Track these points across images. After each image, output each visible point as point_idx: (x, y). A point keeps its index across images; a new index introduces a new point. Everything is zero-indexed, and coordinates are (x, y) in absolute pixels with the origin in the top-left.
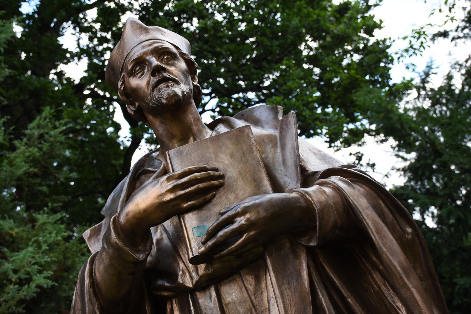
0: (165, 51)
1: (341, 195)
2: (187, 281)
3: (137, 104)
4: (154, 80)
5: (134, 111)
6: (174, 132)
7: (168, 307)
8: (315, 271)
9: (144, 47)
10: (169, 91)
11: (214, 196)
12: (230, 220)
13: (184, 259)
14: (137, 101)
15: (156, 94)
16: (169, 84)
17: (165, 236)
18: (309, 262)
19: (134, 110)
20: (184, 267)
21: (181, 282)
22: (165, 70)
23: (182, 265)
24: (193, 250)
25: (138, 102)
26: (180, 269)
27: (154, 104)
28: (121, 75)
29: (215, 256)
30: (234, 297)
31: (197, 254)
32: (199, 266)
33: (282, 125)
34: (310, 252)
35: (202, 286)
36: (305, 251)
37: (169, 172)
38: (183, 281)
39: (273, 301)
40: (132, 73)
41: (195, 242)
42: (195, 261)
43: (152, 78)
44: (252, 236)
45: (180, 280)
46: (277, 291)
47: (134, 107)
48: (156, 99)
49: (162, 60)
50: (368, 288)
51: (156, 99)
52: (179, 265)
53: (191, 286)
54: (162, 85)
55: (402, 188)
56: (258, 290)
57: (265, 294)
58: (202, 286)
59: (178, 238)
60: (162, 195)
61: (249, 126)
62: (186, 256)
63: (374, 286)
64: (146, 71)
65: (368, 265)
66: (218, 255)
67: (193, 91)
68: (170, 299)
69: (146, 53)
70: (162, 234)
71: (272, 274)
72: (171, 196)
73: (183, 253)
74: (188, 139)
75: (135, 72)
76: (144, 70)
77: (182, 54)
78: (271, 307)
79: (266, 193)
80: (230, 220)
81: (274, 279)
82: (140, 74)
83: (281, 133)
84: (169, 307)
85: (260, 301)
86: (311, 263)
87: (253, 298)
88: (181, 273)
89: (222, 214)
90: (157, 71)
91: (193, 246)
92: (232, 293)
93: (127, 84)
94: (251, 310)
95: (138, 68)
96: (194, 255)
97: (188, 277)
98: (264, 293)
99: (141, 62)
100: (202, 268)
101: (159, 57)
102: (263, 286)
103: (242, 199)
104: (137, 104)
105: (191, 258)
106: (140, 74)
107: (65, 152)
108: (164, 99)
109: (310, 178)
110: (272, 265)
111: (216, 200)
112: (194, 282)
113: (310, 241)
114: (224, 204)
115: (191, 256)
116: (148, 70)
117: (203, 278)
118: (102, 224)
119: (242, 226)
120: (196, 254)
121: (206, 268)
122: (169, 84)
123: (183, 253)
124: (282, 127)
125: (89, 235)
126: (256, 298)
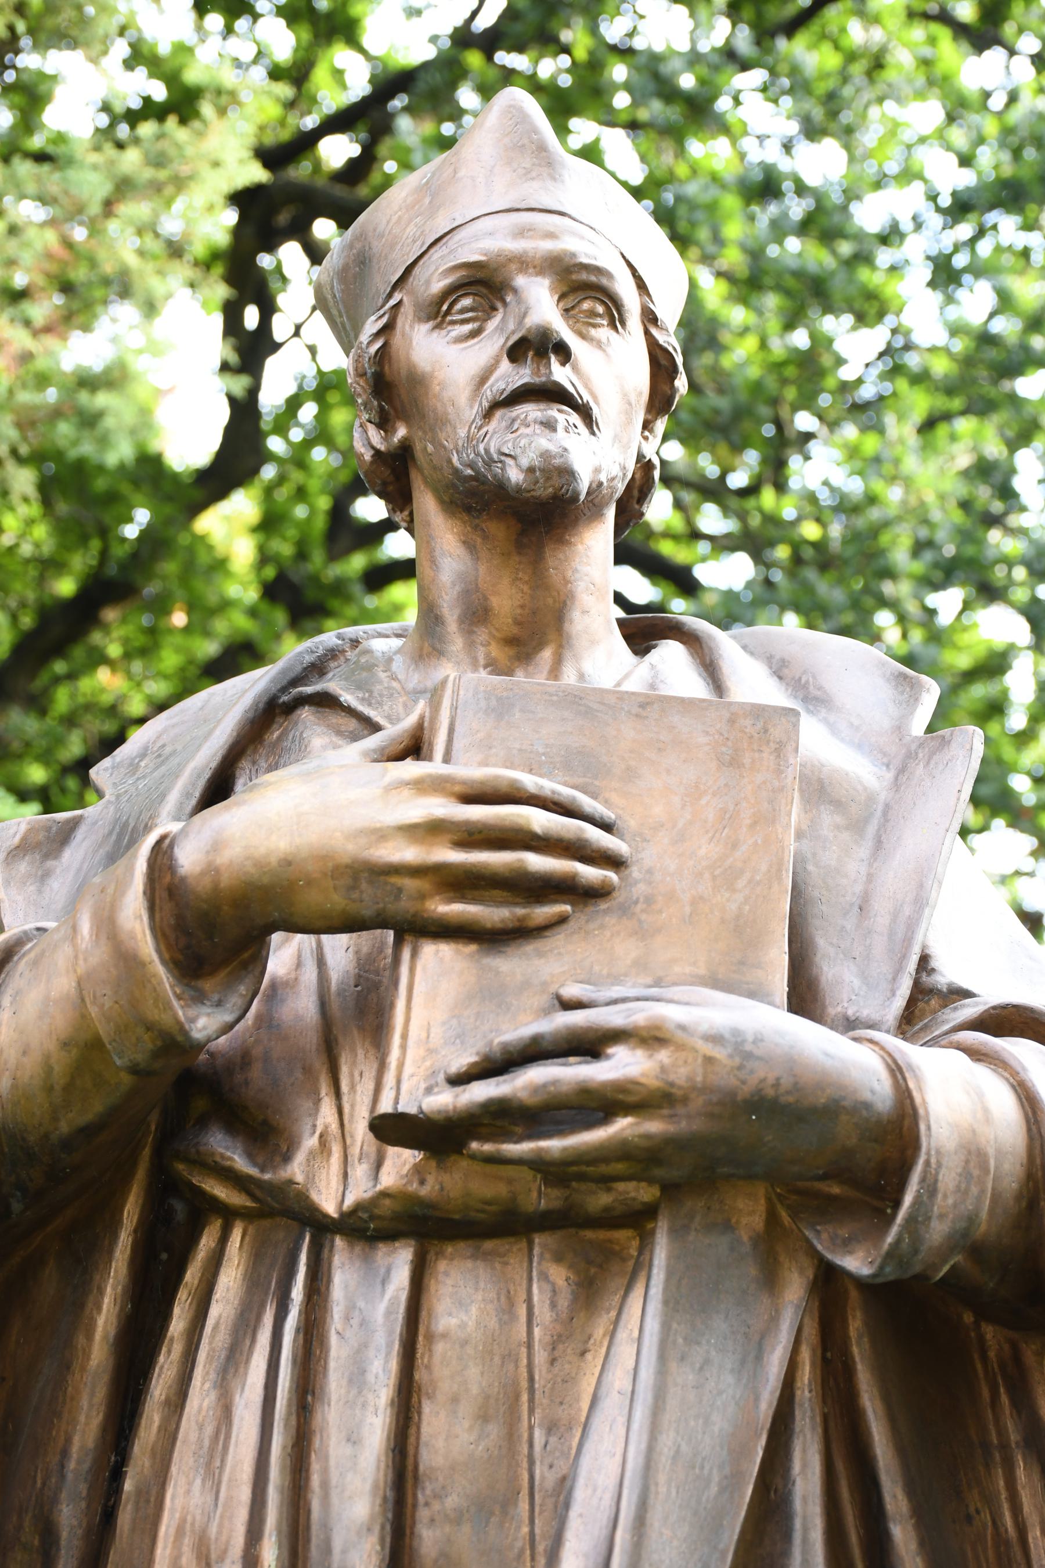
0: (593, 278)
1: (1034, 1128)
2: (322, 1185)
3: (401, 432)
4: (512, 376)
5: (377, 453)
6: (495, 601)
7: (204, 1241)
8: (813, 1364)
9: (521, 232)
10: (544, 442)
11: (562, 920)
12: (589, 1045)
13: (345, 1099)
14: (407, 419)
15: (497, 436)
16: (561, 418)
17: (310, 975)
18: (806, 1320)
19: (382, 447)
20: (334, 1127)
21: (299, 1178)
22: (564, 352)
23: (327, 1114)
24: (405, 1087)
25: (409, 426)
26: (315, 1126)
27: (471, 465)
28: (390, 296)
29: (474, 1145)
30: (471, 1324)
31: (412, 1110)
32: (392, 1151)
33: (910, 756)
34: (828, 1280)
35: (369, 1227)
36: (810, 1274)
37: (430, 758)
38: (310, 1177)
39: (612, 1406)
40: (437, 312)
41: (424, 1059)
42: (392, 1129)
43: (505, 365)
44: (647, 1136)
45: (296, 1170)
46: (647, 1375)
47: (385, 439)
48: (487, 451)
49: (567, 310)
50: (978, 1512)
51: (487, 451)
52: (317, 1110)
53: (330, 1208)
54: (531, 411)
55: (53, 47)
56: (572, 1337)
57: (594, 1362)
58: (369, 1227)
59: (363, 1013)
60: (381, 835)
61: (795, 713)
62: (366, 1087)
63: (1002, 1515)
64: (492, 325)
65: (1010, 1425)
66: (488, 1147)
67: (629, 476)
68: (229, 1215)
69: (524, 263)
70: (299, 965)
71: (655, 1305)
72: (409, 853)
73: (352, 1075)
74: (540, 646)
75: (448, 312)
76: (488, 318)
77: (650, 318)
78: (598, 1424)
79: (756, 993)
80: (589, 1045)
81: (653, 1325)
82: (467, 328)
83: (896, 784)
84: (207, 1242)
85: (564, 1381)
86: (811, 1331)
87: (541, 1357)
88: (310, 1142)
89: (568, 1005)
90: (536, 346)
91: (408, 1069)
92: (466, 1300)
93: (397, 340)
94: (517, 1397)
95: (467, 302)
96: (401, 1109)
97: (338, 1168)
98: (589, 1356)
99: (484, 286)
100: (401, 1162)
101: (562, 297)
102: (599, 1331)
103: (687, 1005)
104: (401, 432)
105: (384, 1117)
106: (467, 328)
107: (124, 540)
108: (518, 466)
109: (934, 1002)
110: (670, 1273)
111: (557, 940)
112: (349, 1201)
113: (847, 1245)
114: (572, 971)
115: (385, 1106)
116: (500, 329)
117: (387, 1202)
118: (81, 817)
119: (621, 1087)
120: (407, 1106)
121: (418, 1171)
122: (561, 418)
123: (352, 1075)
124: (905, 764)
125: (17, 840)
126: (553, 1361)
